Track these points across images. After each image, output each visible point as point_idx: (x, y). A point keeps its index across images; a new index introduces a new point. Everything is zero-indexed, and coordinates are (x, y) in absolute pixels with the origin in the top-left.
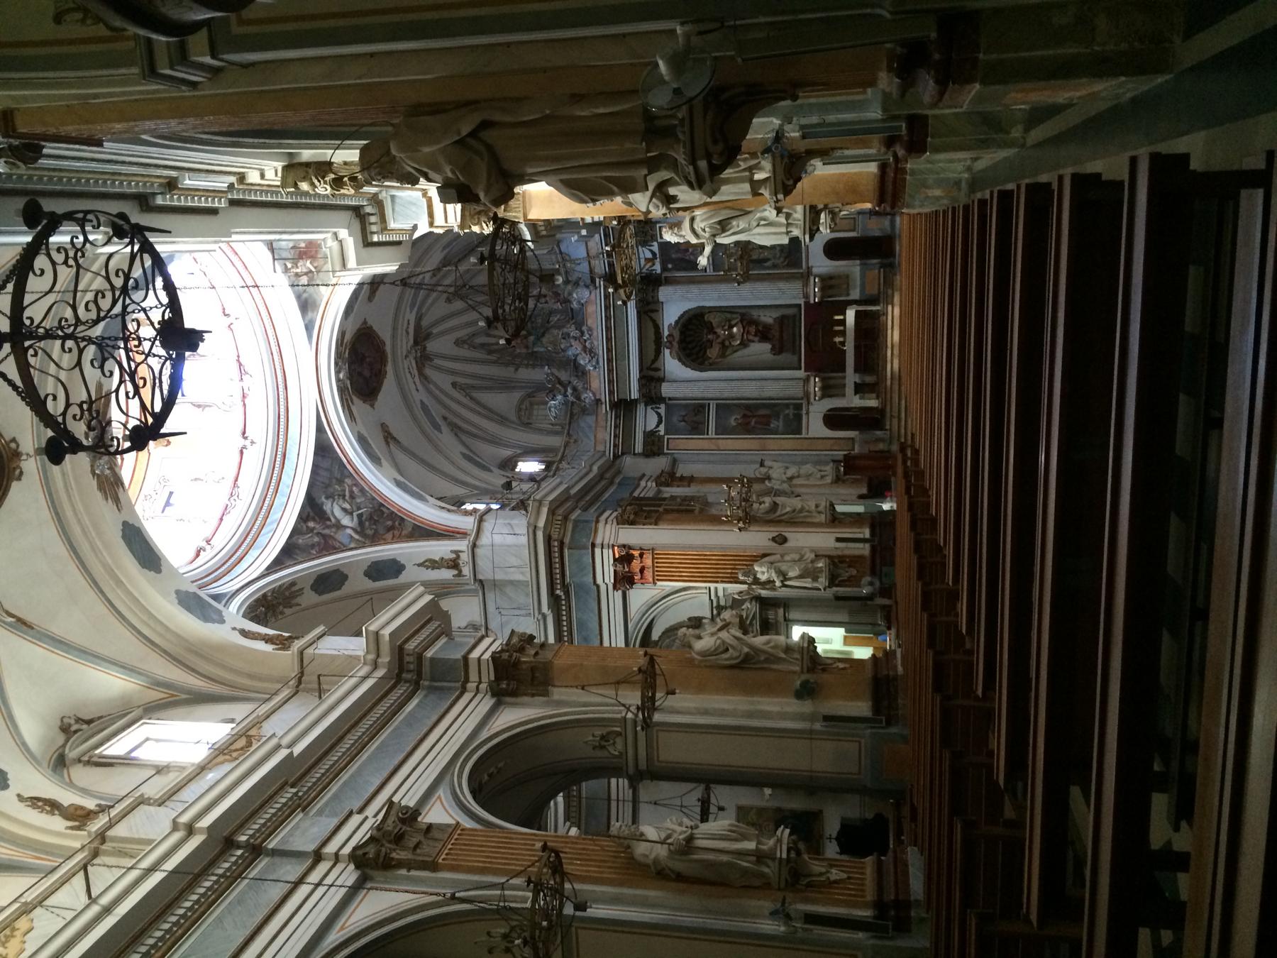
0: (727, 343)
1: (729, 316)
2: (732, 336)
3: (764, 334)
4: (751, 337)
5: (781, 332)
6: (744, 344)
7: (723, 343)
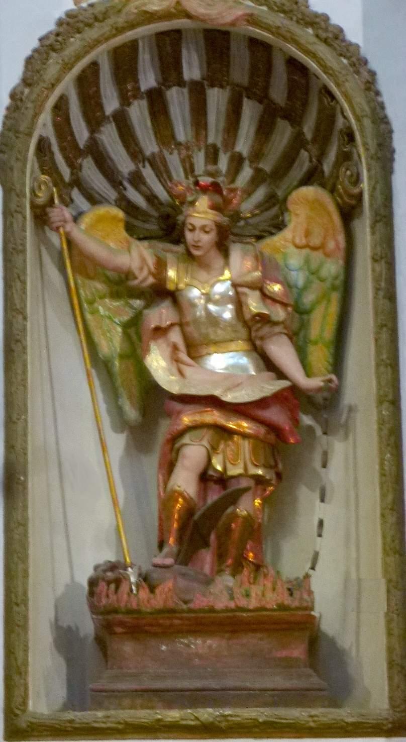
0: (161, 314)
1: (321, 325)
2: (194, 349)
3: (205, 529)
4: (193, 453)
5: (231, 624)
6: (149, 415)
7: (162, 293)
